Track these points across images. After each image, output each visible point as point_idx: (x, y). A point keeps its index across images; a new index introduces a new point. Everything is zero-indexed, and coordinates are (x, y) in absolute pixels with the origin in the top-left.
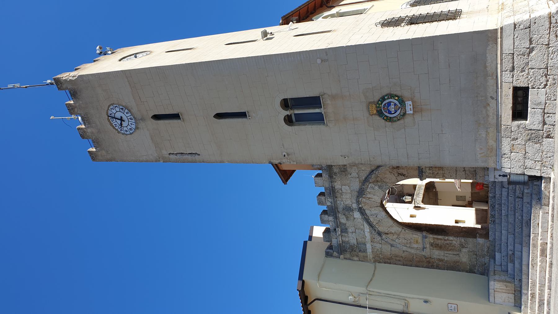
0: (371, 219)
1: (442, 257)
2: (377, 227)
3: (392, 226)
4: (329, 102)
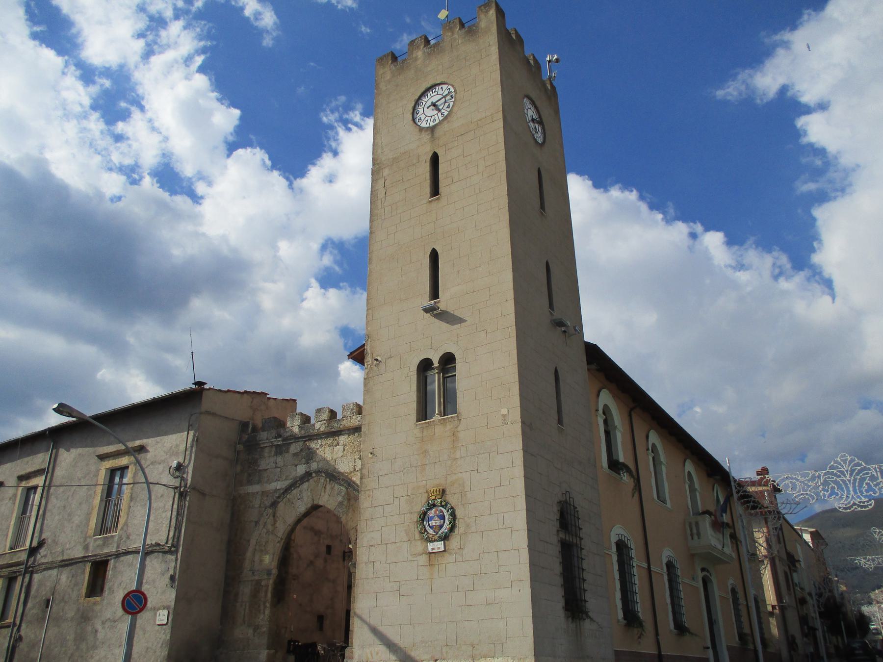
0: (295, 492)
3: (118, 547)
4: (449, 427)
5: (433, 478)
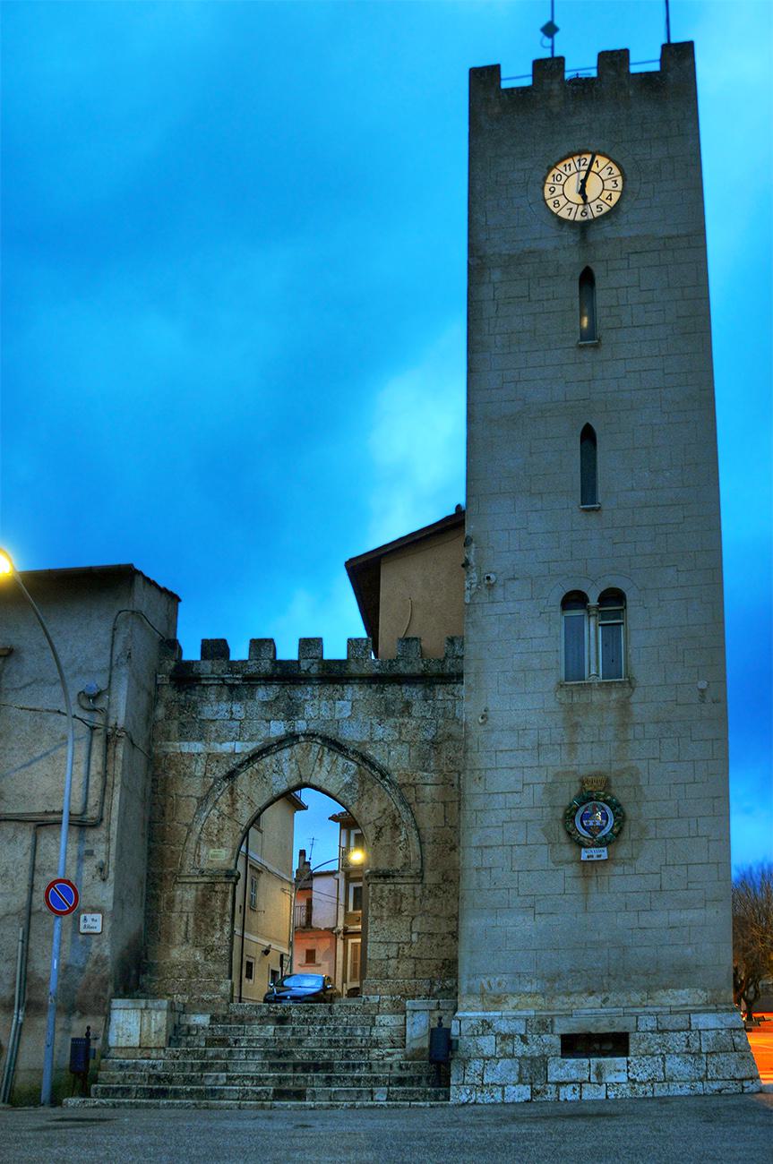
0: (267, 760)
1: (177, 907)
2: (249, 771)
3: (251, 803)
5: (590, 759)
